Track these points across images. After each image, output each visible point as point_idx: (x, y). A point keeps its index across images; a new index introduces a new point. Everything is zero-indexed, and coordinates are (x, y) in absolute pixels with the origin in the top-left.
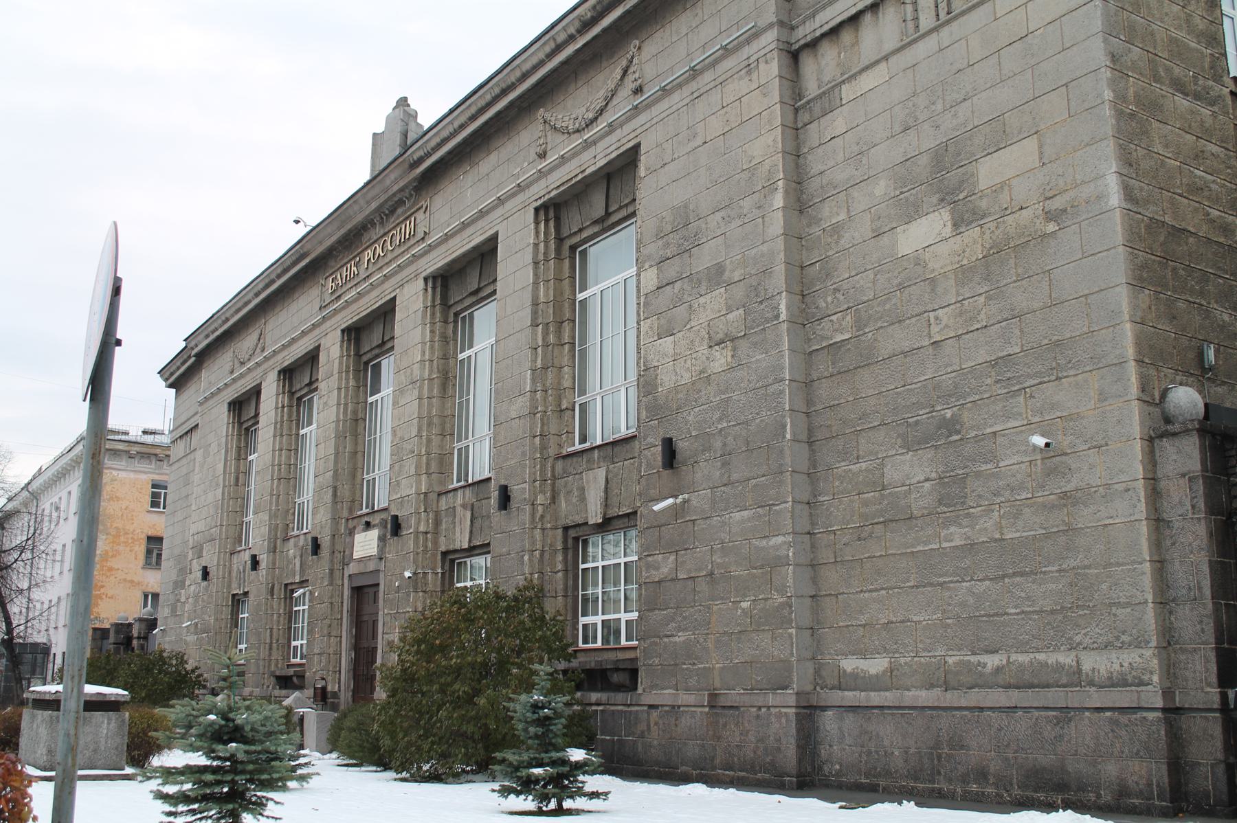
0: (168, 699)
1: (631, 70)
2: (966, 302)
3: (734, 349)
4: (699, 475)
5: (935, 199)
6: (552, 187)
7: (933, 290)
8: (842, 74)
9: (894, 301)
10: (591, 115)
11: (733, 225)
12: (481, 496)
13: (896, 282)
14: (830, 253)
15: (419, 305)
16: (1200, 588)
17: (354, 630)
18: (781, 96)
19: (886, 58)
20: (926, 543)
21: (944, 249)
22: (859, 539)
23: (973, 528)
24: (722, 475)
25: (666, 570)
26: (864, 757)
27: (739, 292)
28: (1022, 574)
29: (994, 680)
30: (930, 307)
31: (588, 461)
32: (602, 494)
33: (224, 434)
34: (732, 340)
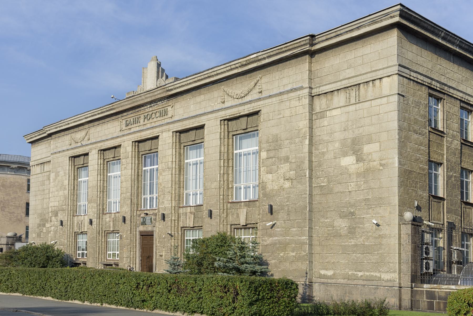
0: (100, 273)
1: (258, 84)
2: (358, 182)
3: (292, 182)
4: (280, 217)
5: (352, 152)
6: (227, 115)
7: (350, 177)
8: (327, 108)
9: (339, 178)
10: (243, 95)
11: (292, 145)
12: (198, 210)
13: (340, 172)
14: (321, 160)
15: (170, 141)
16: (409, 260)
17: (141, 250)
18: (309, 110)
19: (340, 107)
20: (345, 243)
21: (353, 167)
22: (326, 240)
23: (357, 240)
24: (287, 217)
25: (269, 242)
26: (326, 296)
27: (294, 166)
28: (369, 253)
29: (361, 278)
30: (349, 181)
31: (240, 206)
32: (245, 217)
33: (68, 169)
34: (291, 179)
